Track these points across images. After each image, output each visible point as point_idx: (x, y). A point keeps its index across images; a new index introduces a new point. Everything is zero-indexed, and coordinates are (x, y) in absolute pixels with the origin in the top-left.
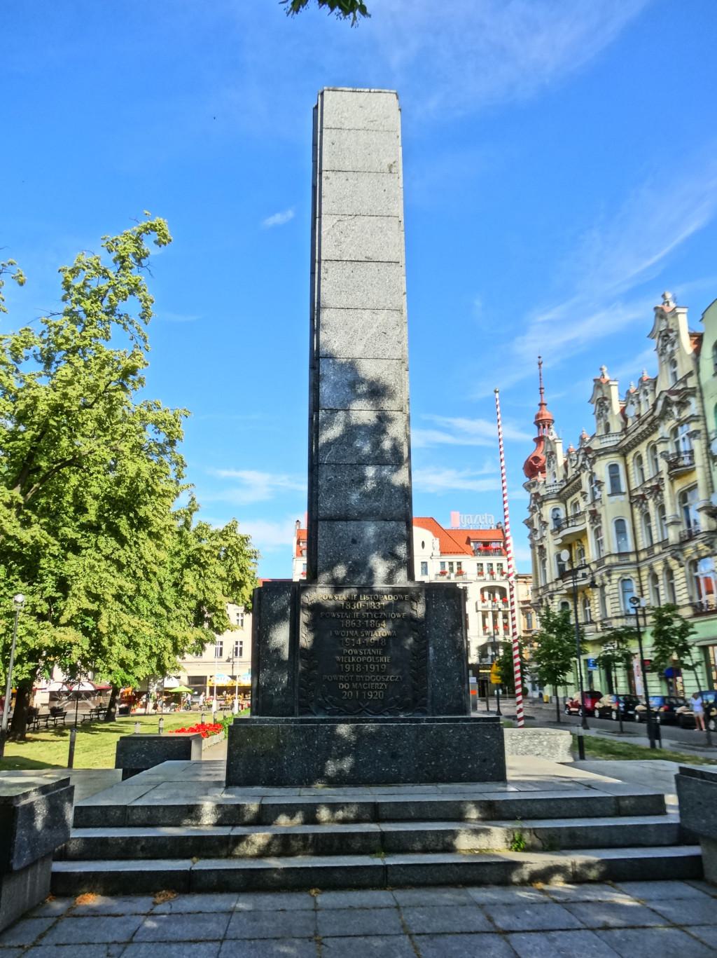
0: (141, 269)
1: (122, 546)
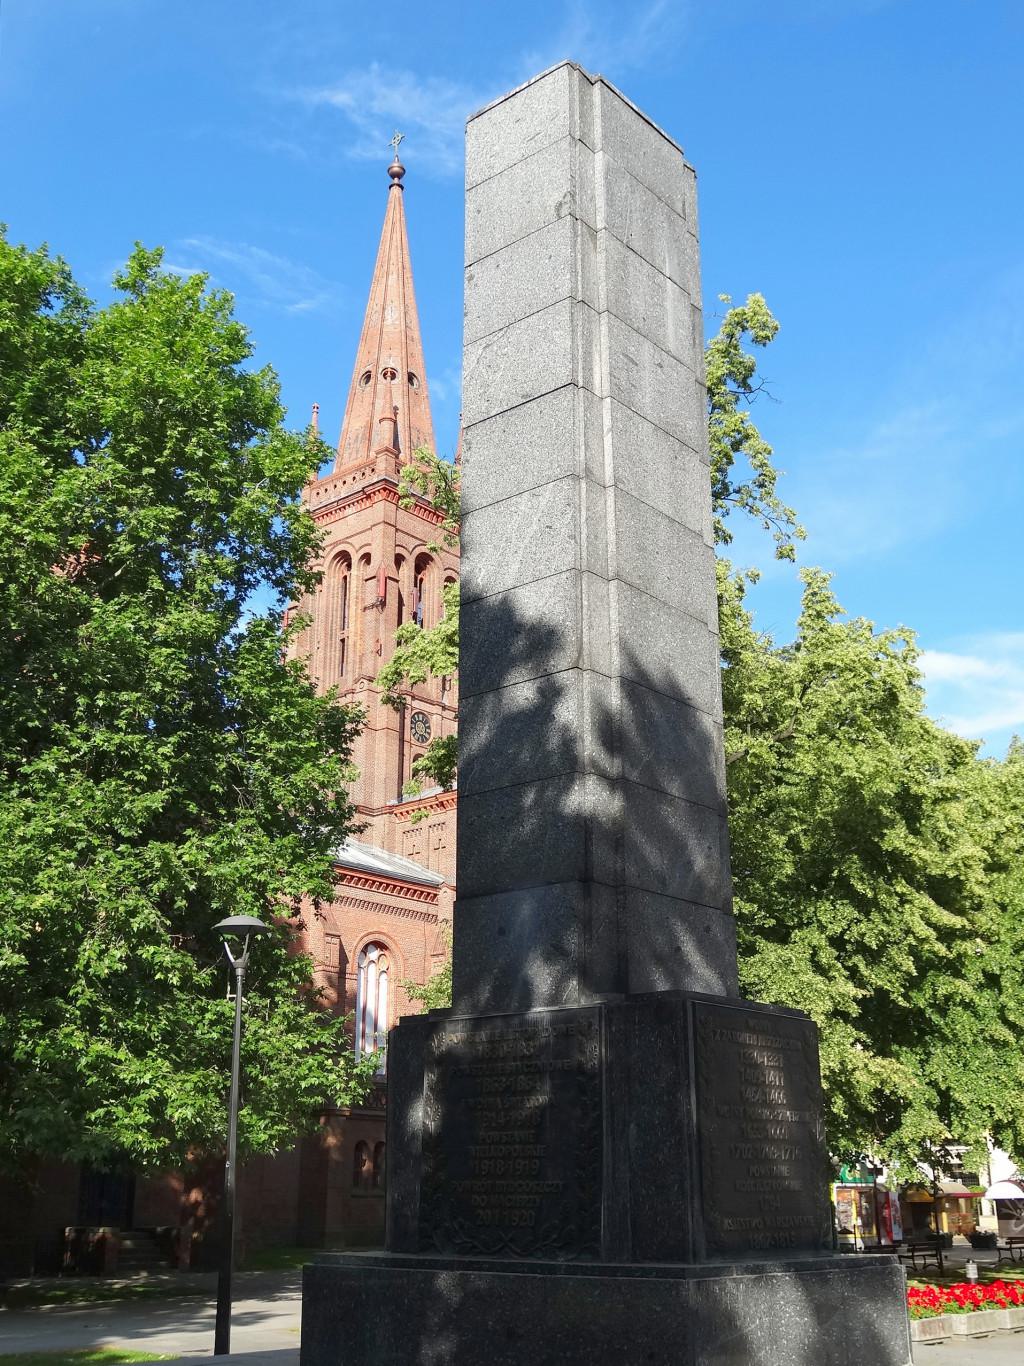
0: (751, 396)
1: (867, 914)
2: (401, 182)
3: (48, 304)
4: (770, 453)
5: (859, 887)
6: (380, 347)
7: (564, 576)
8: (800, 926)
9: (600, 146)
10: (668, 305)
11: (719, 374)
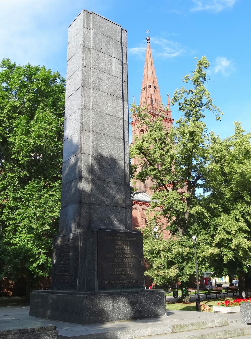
0: (206, 81)
2: (149, 41)
3: (56, 82)
4: (210, 95)
5: (246, 199)
6: (147, 81)
7: (79, 132)
8: (233, 209)
9: (92, 29)
10: (114, 64)
11: (197, 77)
